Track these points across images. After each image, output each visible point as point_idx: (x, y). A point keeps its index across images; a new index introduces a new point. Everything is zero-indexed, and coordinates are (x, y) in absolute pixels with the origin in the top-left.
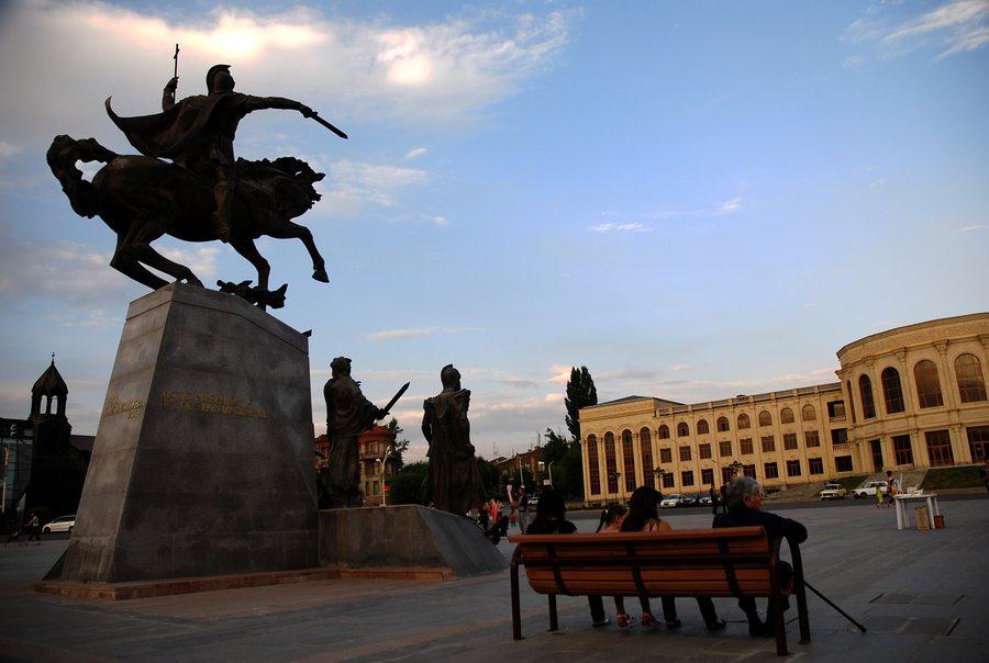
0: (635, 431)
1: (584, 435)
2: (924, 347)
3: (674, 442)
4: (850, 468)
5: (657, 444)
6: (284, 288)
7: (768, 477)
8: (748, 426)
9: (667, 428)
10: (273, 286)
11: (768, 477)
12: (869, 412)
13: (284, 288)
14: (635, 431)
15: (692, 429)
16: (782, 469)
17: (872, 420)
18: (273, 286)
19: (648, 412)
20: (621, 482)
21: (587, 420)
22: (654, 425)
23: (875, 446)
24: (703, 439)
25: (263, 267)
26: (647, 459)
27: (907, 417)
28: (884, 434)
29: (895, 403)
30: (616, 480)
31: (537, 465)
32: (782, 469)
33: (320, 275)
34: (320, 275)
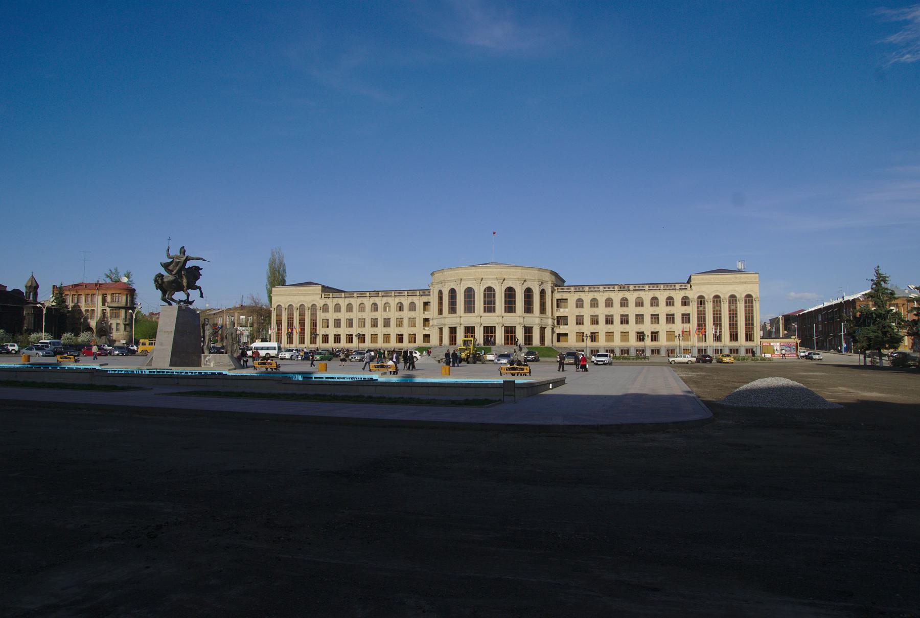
0: (725, 296)
1: (274, 305)
2: (492, 279)
3: (331, 316)
4: (429, 342)
5: (320, 316)
6: (194, 301)
7: (335, 342)
8: (582, 306)
9: (612, 300)
10: (190, 300)
11: (335, 342)
12: (453, 309)
13: (194, 301)
14: (725, 296)
15: (343, 308)
16: (343, 339)
17: (441, 316)
18: (190, 300)
19: (317, 294)
20: (296, 337)
21: (277, 295)
22: (320, 303)
23: (453, 330)
24: (349, 315)
25: (188, 295)
26: (314, 325)
27: (456, 317)
28: (444, 325)
29: (470, 308)
30: (316, 338)
31: (239, 318)
32: (343, 339)
33: (202, 296)
34: (202, 296)
